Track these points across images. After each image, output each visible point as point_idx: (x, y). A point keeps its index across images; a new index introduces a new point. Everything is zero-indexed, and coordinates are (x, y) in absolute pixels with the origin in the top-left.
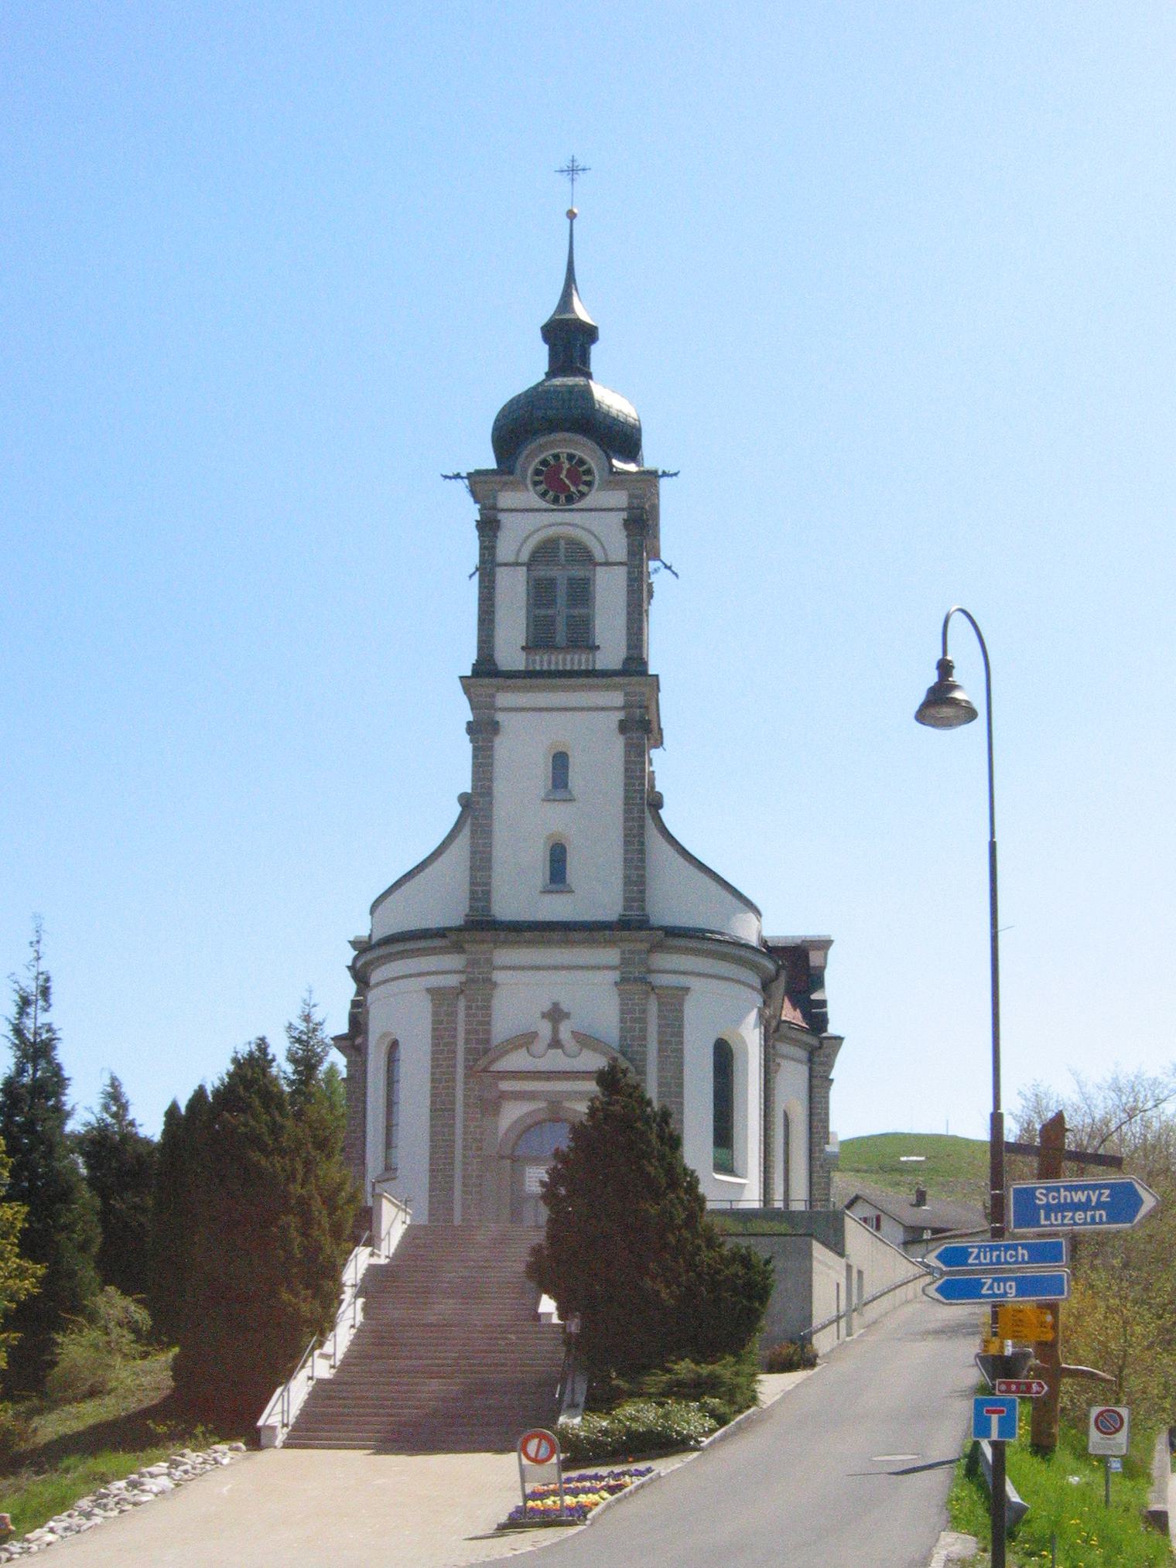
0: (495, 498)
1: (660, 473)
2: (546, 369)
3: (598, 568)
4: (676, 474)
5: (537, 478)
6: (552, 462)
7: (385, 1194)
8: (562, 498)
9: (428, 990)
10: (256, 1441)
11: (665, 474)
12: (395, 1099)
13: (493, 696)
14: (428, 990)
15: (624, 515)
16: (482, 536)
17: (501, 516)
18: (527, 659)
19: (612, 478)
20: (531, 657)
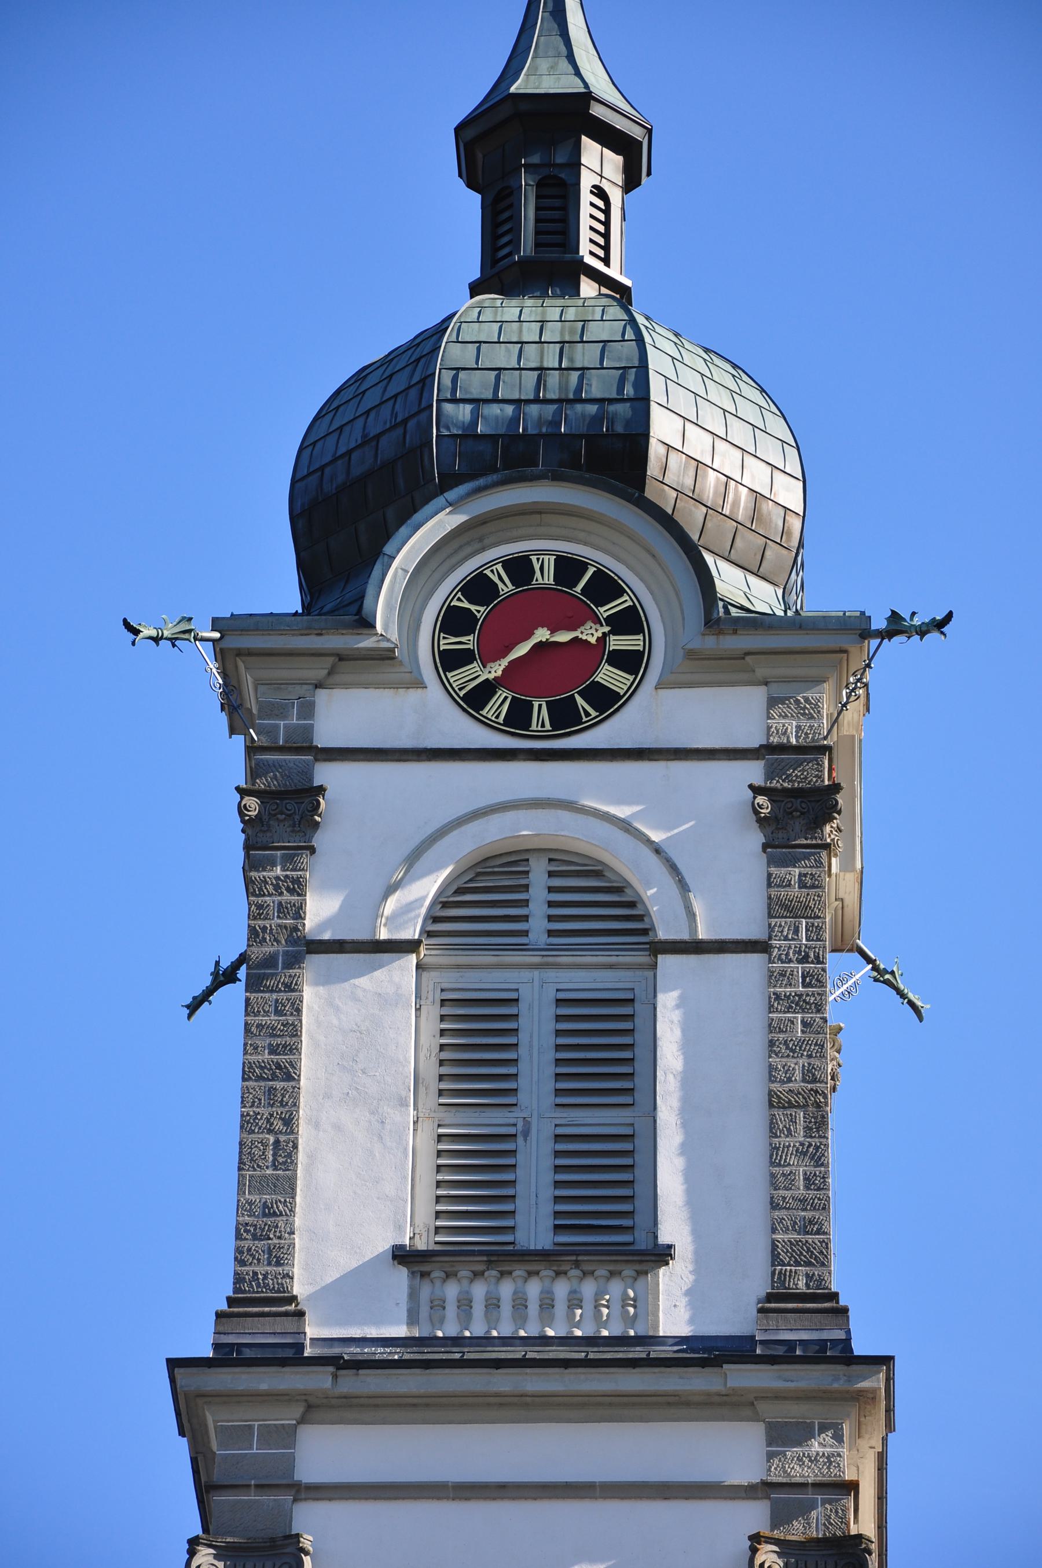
0: (308, 709)
1: (879, 623)
2: (477, 274)
3: (666, 961)
4: (940, 625)
5: (449, 642)
6: (506, 587)
7: (479, 660)
8: (540, 714)
9: (609, 267)
10: (769, 866)
11: (896, 627)
12: (838, 649)
13: (288, 1436)
14: (609, 267)
15: (754, 772)
16: (254, 894)
17: (326, 774)
18: (413, 1295)
19: (711, 642)
20: (426, 1291)
